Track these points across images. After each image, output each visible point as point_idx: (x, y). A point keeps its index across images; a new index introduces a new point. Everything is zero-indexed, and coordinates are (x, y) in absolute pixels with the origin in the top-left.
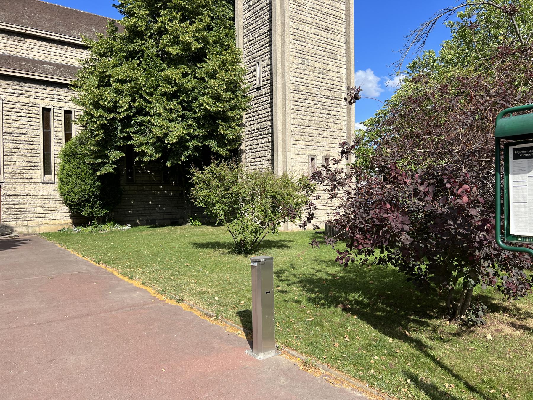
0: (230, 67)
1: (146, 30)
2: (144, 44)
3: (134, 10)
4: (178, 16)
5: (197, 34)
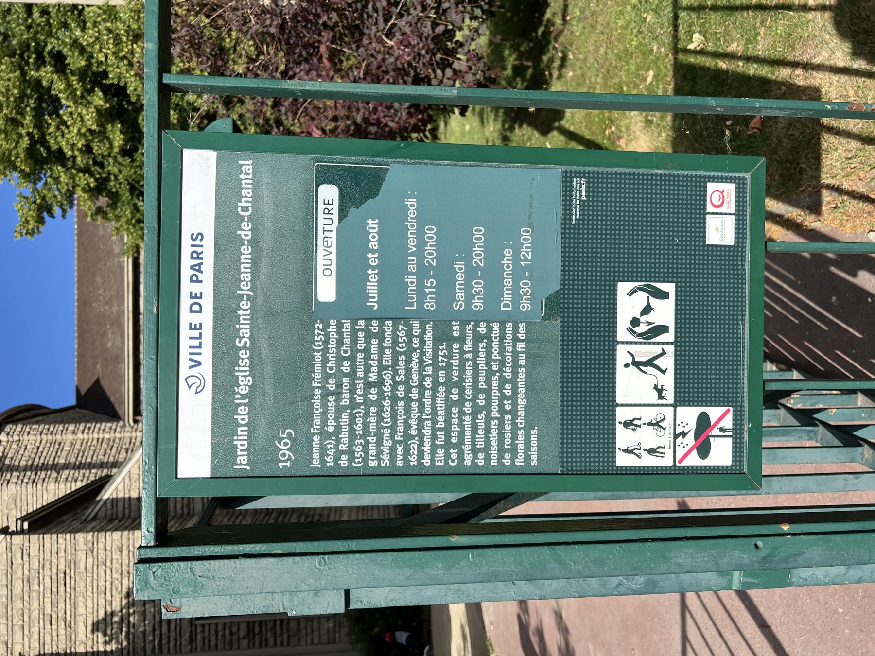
0: (126, 50)
1: (92, 175)
2: (116, 177)
3: (63, 191)
4: (53, 124)
5: (78, 93)
